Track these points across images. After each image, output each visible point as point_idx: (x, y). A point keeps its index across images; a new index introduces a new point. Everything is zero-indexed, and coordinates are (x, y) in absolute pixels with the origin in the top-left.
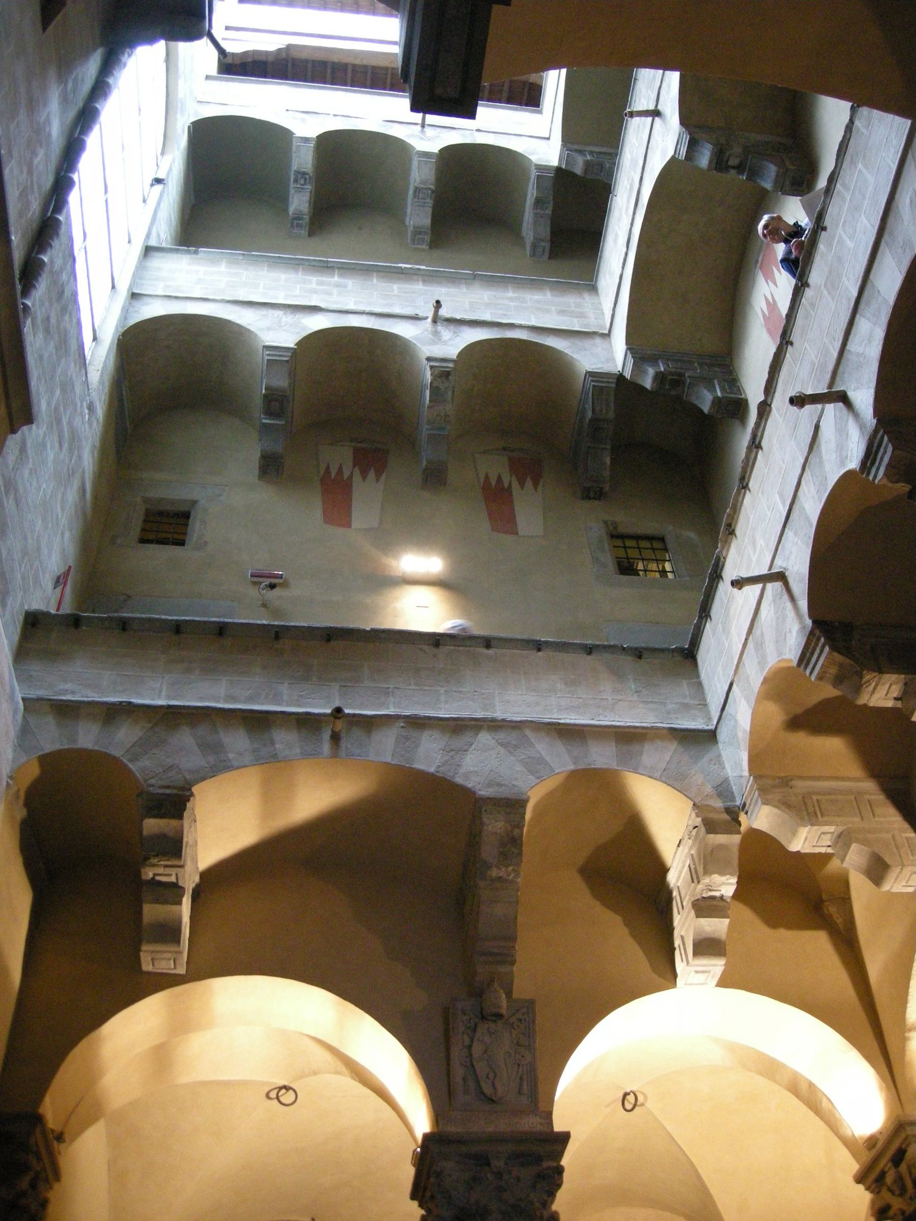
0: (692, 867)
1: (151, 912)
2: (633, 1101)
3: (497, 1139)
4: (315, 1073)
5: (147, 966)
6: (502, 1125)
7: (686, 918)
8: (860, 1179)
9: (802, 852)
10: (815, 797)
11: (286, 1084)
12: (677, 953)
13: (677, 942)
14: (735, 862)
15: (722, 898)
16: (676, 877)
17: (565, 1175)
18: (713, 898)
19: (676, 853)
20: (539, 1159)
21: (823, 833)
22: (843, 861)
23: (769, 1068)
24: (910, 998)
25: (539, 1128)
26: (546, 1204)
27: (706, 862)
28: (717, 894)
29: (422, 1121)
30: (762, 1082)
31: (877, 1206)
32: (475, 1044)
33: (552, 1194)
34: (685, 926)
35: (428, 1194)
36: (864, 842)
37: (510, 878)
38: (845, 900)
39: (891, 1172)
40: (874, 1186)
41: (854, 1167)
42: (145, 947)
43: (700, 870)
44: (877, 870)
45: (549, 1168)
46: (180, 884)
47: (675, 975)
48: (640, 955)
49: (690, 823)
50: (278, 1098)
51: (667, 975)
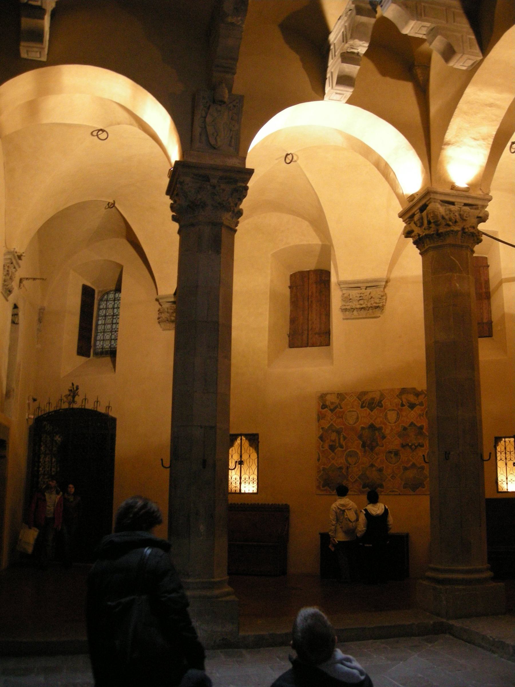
0: (345, 33)
1: (26, 23)
2: (291, 159)
3: (215, 168)
4: (119, 124)
5: (24, 55)
6: (218, 161)
7: (336, 62)
8: (401, 216)
9: (409, 35)
10: (423, 4)
11: (102, 128)
12: (327, 81)
13: (328, 75)
14: (370, 34)
15: (358, 54)
16: (334, 38)
17: (249, 191)
18: (353, 53)
19: (336, 24)
20: (236, 181)
21: (423, 26)
22: (431, 44)
23: (366, 152)
24: (449, 127)
25: (238, 165)
26: (237, 205)
27: (353, 31)
28: (356, 51)
29: (175, 154)
30: (361, 159)
31: (407, 231)
32: (208, 116)
33: (241, 200)
34: (335, 66)
35: (175, 193)
36: (445, 36)
37: (239, 24)
38: (427, 67)
39: (417, 215)
40: (407, 220)
41: (400, 209)
42: (23, 44)
43: (349, 36)
44: (449, 53)
45: (241, 186)
46: (44, 7)
47: (324, 93)
48: (307, 79)
49: (348, 7)
50: (97, 135)
51: (318, 92)
